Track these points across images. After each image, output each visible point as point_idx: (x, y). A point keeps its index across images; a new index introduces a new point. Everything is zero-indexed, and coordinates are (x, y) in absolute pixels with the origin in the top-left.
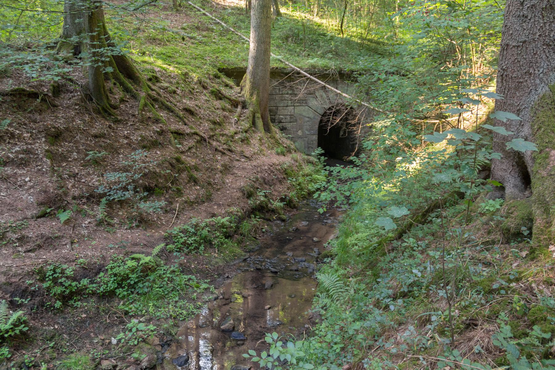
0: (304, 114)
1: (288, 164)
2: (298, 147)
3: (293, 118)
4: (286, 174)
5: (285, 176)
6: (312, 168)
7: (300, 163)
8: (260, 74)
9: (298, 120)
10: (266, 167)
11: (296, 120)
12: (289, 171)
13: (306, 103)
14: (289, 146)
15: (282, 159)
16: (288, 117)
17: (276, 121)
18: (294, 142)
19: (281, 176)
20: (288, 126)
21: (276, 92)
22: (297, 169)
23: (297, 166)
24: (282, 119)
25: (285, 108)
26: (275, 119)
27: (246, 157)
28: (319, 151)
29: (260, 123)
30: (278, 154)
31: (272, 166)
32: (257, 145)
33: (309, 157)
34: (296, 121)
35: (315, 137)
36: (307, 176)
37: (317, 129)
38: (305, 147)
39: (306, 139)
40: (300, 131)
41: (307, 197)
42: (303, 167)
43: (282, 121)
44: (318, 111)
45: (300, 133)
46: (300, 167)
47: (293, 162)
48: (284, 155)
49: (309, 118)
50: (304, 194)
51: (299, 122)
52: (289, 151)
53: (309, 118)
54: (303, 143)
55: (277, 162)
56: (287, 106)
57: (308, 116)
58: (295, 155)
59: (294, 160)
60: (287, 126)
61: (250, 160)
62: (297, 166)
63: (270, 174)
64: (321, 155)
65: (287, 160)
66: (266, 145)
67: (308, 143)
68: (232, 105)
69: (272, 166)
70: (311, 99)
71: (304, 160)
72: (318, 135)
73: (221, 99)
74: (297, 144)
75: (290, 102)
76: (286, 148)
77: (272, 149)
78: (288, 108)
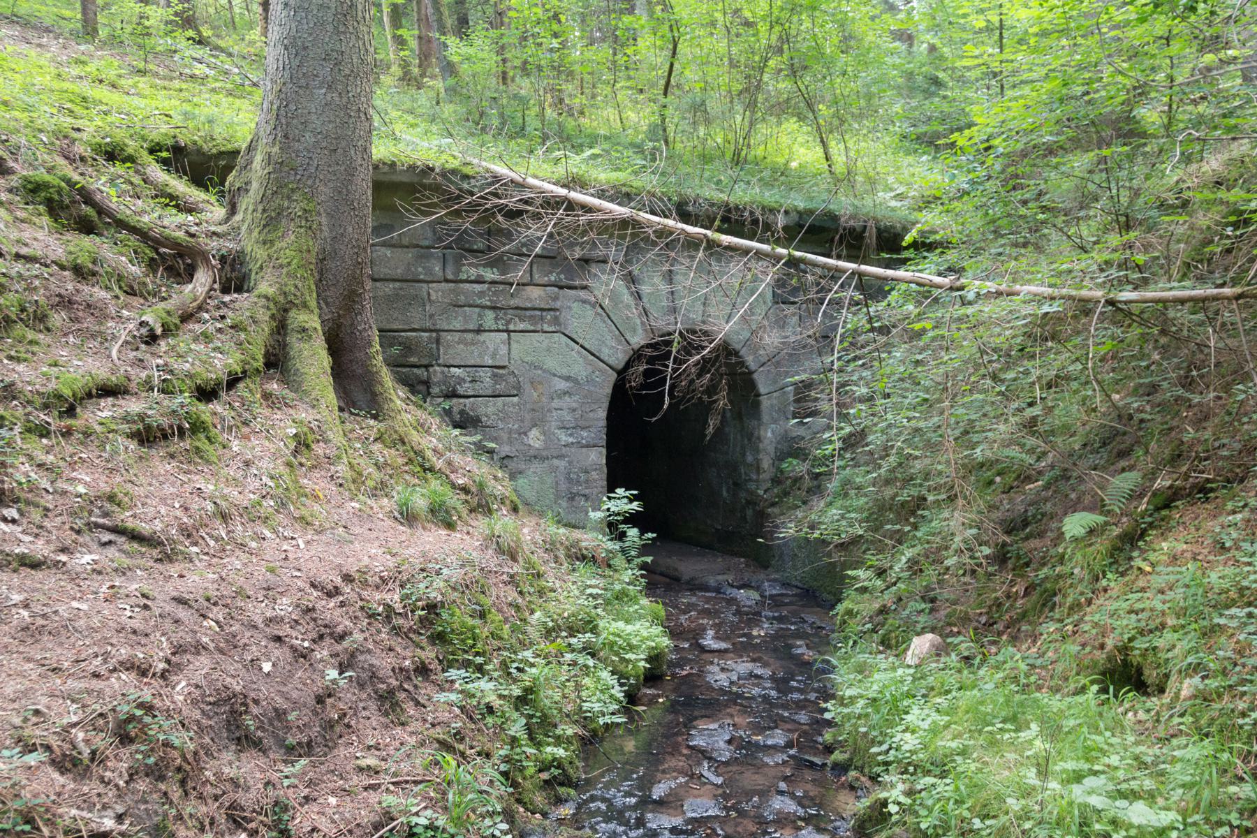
0: (551, 363)
1: (454, 573)
2: (530, 495)
3: (506, 383)
4: (439, 638)
5: (429, 654)
6: (596, 584)
7: (530, 565)
8: (316, 122)
9: (527, 387)
10: (285, 606)
11: (518, 387)
12: (458, 617)
13: (556, 321)
14: (481, 487)
15: (431, 541)
16: (485, 374)
17: (435, 390)
18: (513, 477)
19: (386, 659)
20: (488, 409)
21: (429, 271)
22: (512, 595)
23: (512, 580)
24: (461, 381)
25: (470, 336)
26: (427, 383)
27: (135, 536)
28: (623, 502)
29: (313, 359)
30: (408, 517)
31: (333, 592)
32: (265, 464)
33: (577, 534)
34: (517, 391)
35: (597, 457)
36: (572, 632)
37: (604, 423)
38: (558, 496)
39: (562, 464)
40: (534, 433)
41: (578, 771)
42: (550, 581)
43: (461, 391)
44: (605, 353)
45: (535, 439)
46: (531, 584)
47: (490, 559)
48: (450, 526)
49: (568, 379)
50: (557, 763)
51: (531, 394)
52: (482, 505)
53: (568, 379)
54: (549, 480)
55: (382, 563)
56: (479, 331)
57: (565, 371)
58: (503, 522)
59: (500, 550)
60: (481, 411)
61: (168, 558)
62: (512, 580)
63: (302, 655)
64: (632, 519)
65: (447, 555)
66: (342, 469)
67: (569, 480)
68: (152, 265)
69: (333, 592)
70: (576, 306)
71: (550, 547)
72: (611, 446)
73: (87, 227)
74: (521, 481)
75: (490, 315)
76: (465, 490)
77: (381, 489)
78: (483, 337)
